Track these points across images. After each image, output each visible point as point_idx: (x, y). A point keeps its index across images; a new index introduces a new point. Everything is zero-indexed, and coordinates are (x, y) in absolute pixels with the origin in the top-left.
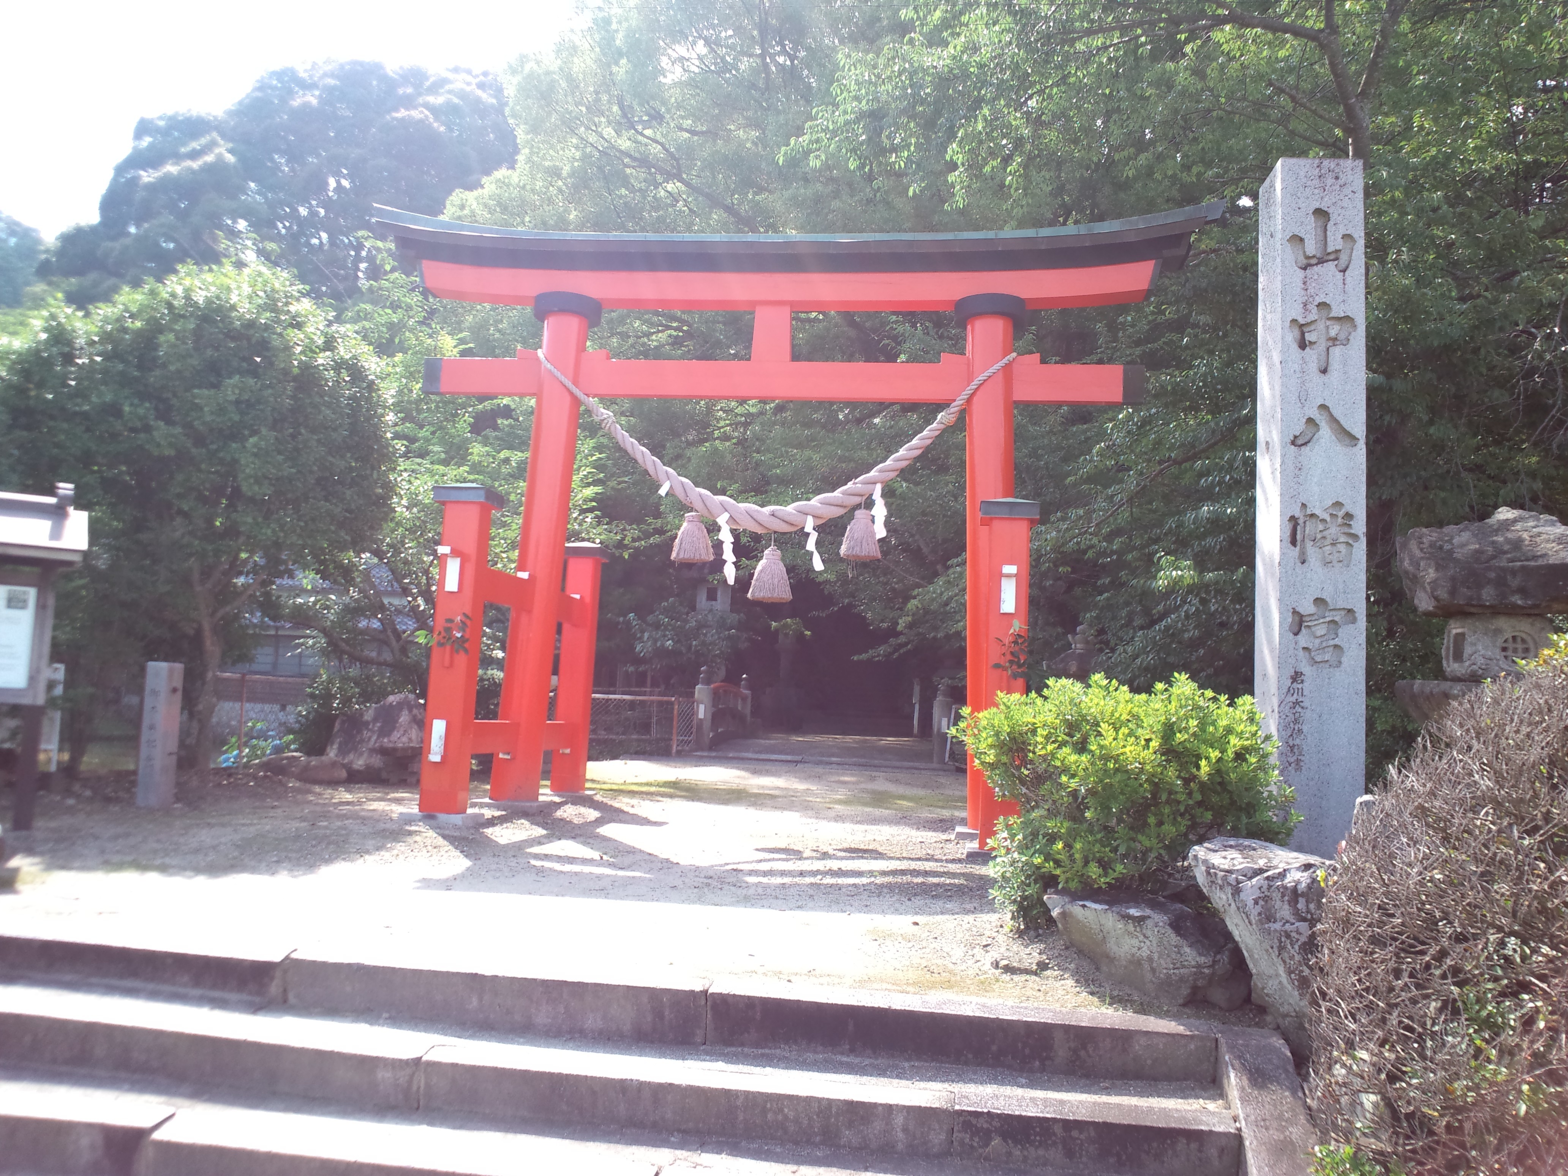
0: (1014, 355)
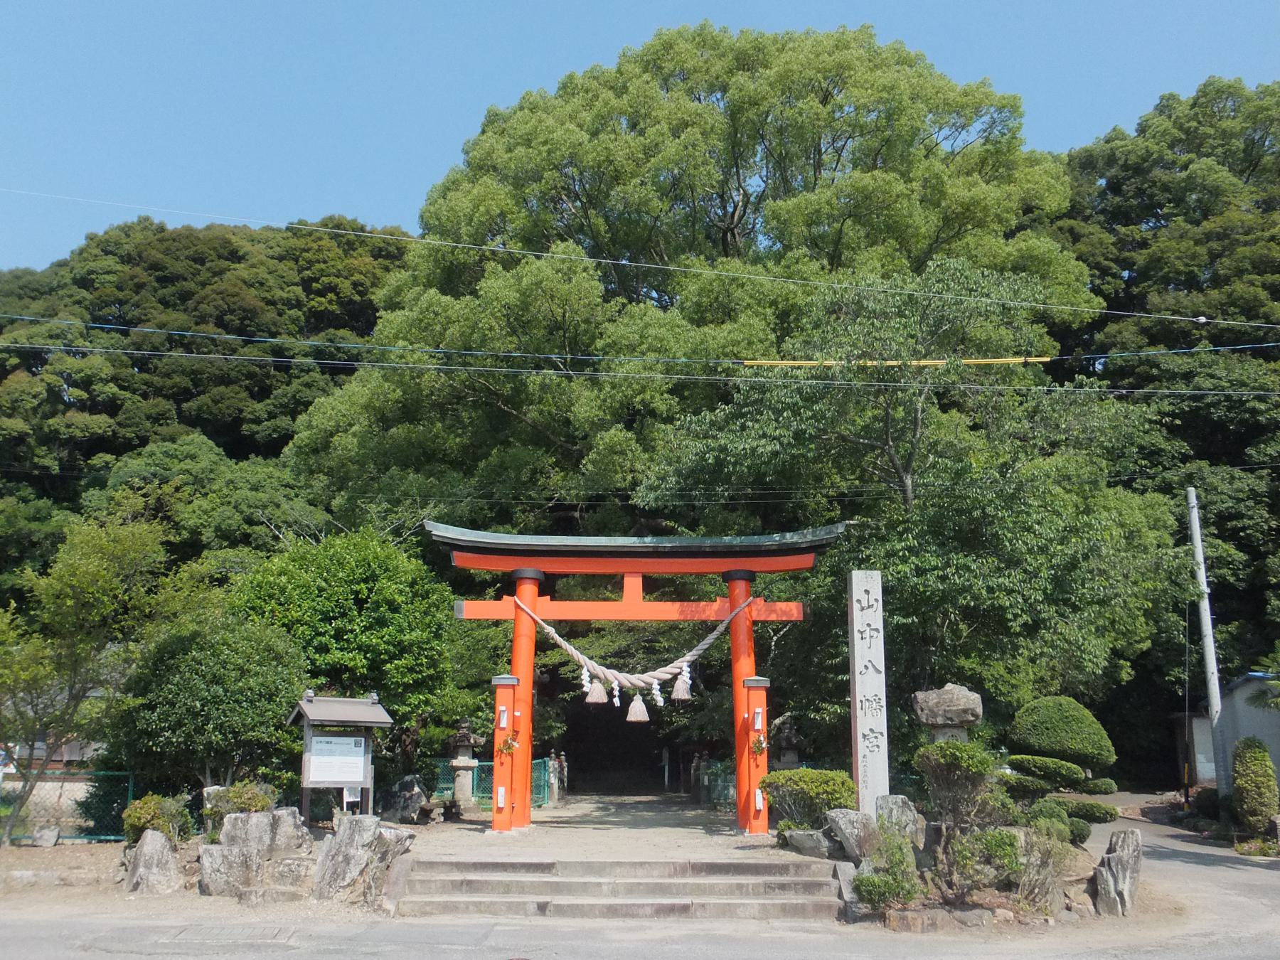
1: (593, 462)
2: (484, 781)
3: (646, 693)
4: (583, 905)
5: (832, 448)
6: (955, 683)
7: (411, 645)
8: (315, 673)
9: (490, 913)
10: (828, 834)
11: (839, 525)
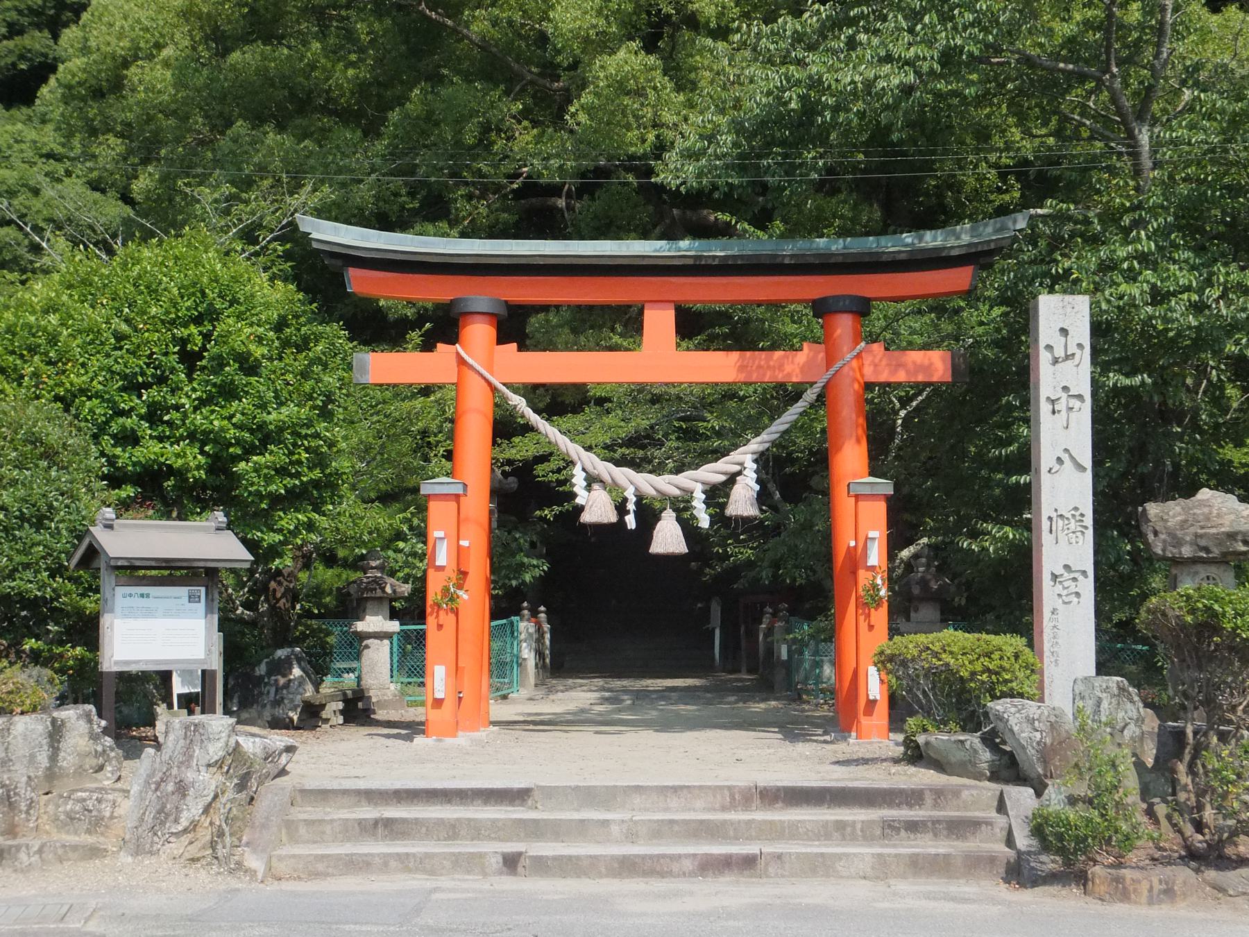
0: (863, 344)
1: (589, 110)
2: (411, 657)
3: (682, 507)
4: (578, 858)
5: (1009, 79)
6: (1216, 488)
7: (281, 430)
8: (115, 480)
9: (425, 871)
10: (991, 740)
11: (1019, 216)
